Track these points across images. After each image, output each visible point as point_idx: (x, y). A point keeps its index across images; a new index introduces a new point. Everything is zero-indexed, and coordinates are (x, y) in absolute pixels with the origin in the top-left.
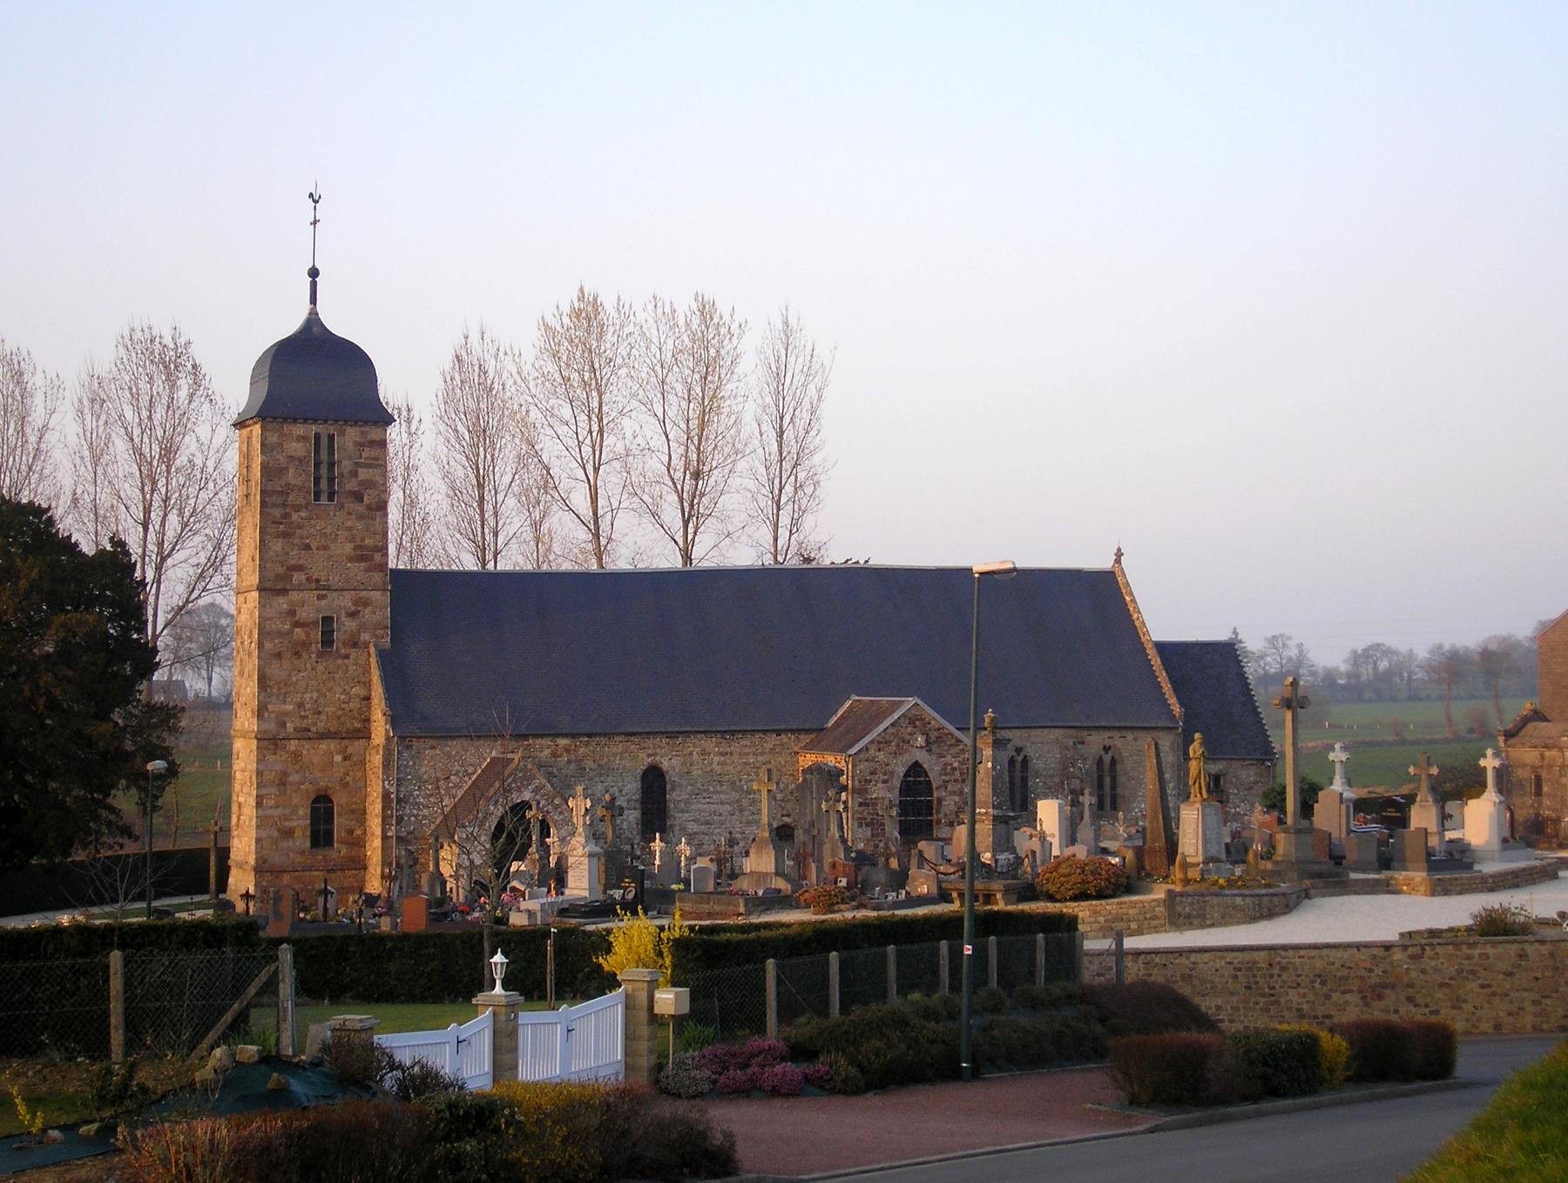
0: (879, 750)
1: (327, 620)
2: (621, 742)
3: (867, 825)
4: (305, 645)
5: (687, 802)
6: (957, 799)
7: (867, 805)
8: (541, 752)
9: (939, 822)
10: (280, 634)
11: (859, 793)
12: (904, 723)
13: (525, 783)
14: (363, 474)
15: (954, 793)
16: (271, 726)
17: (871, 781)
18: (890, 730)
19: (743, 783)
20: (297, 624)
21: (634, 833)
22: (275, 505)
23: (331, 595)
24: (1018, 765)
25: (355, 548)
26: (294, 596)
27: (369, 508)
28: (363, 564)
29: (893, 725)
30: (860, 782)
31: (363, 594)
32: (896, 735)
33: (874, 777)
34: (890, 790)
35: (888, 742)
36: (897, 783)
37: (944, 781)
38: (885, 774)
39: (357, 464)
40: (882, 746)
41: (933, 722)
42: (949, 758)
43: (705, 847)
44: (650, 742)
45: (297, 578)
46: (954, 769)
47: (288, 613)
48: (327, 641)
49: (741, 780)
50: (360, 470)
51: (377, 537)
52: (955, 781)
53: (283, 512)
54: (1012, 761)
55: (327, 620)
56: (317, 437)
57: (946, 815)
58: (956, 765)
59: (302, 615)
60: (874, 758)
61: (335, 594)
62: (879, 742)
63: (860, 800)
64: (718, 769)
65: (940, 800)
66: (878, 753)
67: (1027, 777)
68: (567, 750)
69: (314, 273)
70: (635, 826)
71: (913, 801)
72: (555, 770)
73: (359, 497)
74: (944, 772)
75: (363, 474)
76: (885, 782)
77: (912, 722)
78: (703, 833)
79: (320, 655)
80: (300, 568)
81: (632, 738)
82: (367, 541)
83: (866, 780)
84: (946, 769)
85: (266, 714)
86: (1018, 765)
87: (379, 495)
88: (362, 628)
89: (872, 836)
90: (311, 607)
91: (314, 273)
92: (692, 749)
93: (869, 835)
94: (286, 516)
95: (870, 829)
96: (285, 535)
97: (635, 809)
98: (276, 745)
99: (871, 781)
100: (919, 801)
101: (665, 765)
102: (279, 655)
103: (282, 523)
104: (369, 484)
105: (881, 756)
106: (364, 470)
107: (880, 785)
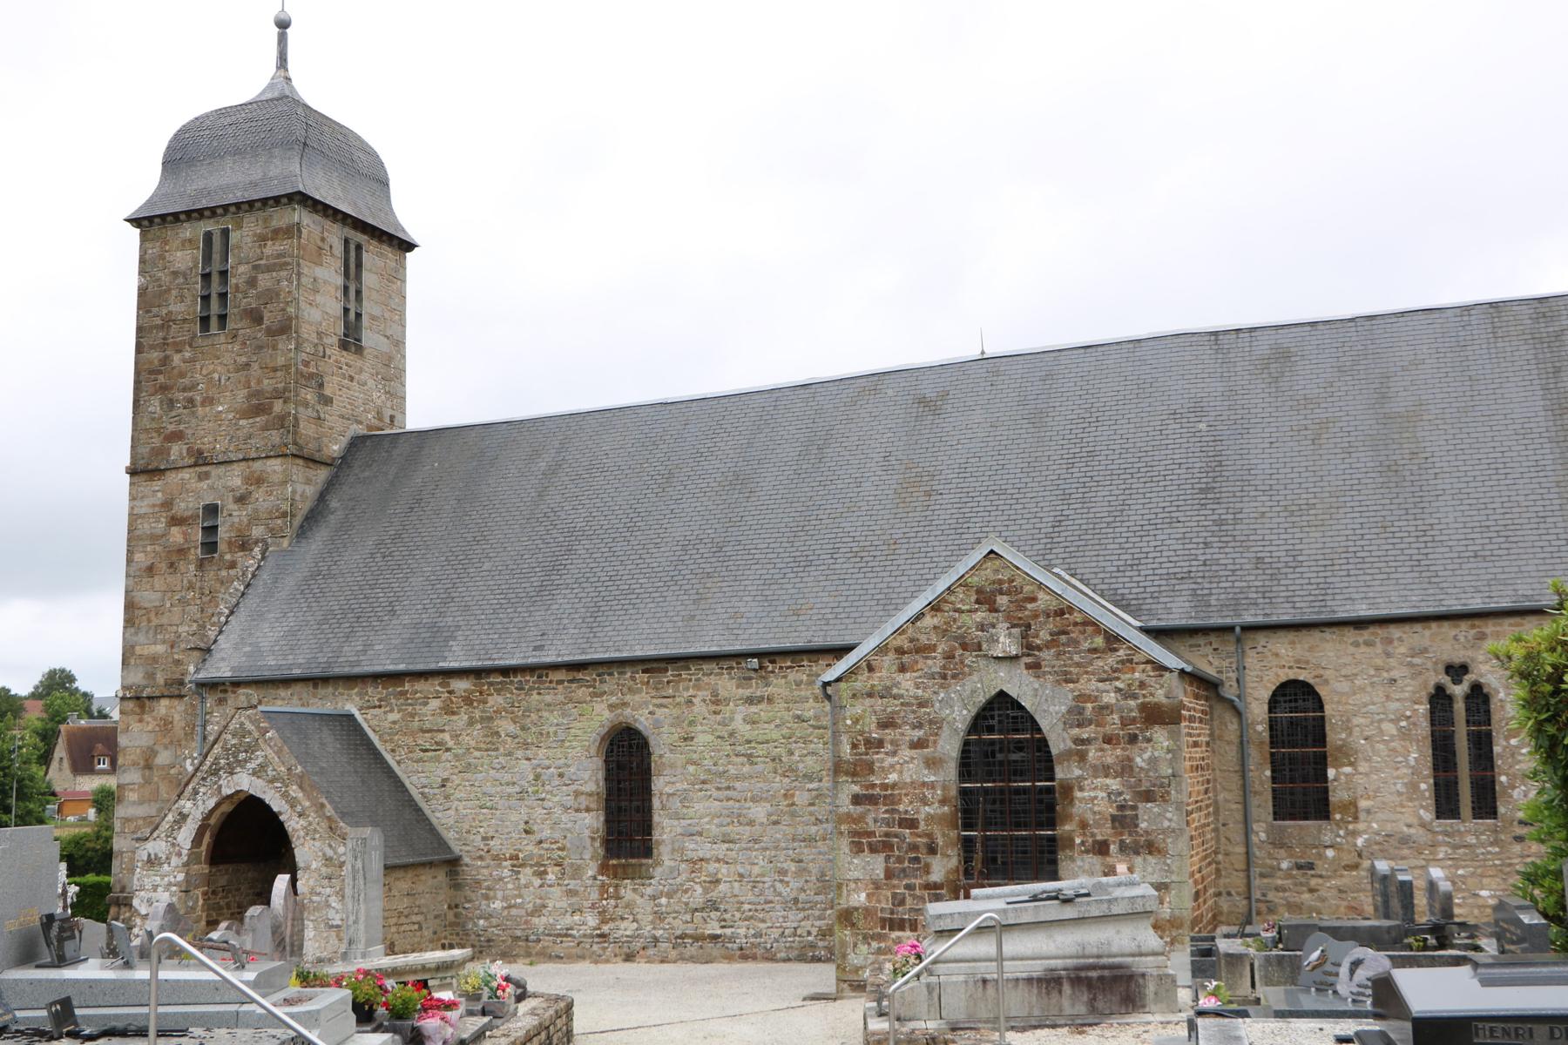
0: (902, 669)
1: (212, 510)
2: (560, 682)
3: (873, 849)
4: (182, 552)
5: (685, 799)
6: (1114, 784)
7: (872, 800)
8: (426, 704)
9: (1070, 843)
10: (154, 538)
11: (854, 774)
12: (964, 600)
13: (242, 756)
14: (264, 281)
15: (1106, 770)
16: (137, 677)
17: (880, 743)
18: (929, 621)
19: (796, 758)
20: (175, 521)
21: (587, 856)
22: (152, 347)
23: (215, 471)
24: (1459, 707)
25: (249, 396)
26: (173, 478)
27: (271, 332)
28: (258, 419)
29: (935, 607)
30: (854, 746)
31: (257, 465)
32: (942, 632)
33: (889, 734)
34: (932, 763)
35: (924, 650)
36: (949, 746)
37: (1079, 741)
38: (920, 726)
39: (256, 267)
40: (906, 659)
41: (1041, 595)
42: (1089, 685)
43: (722, 887)
44: (610, 683)
45: (177, 450)
46: (1104, 709)
47: (162, 505)
48: (210, 547)
49: (791, 753)
50: (260, 277)
51: (279, 374)
52: (1108, 740)
53: (162, 355)
54: (1440, 699)
55: (212, 510)
56: (208, 237)
57: (1084, 825)
58: (1110, 698)
59: (183, 506)
60: (888, 689)
61: (222, 469)
62: (900, 651)
63: (856, 789)
64: (744, 730)
65: (1067, 789)
66: (900, 677)
67: (1489, 735)
68: (468, 701)
69: (283, 25)
70: (588, 841)
71: (1002, 791)
72: (446, 737)
73: (256, 317)
74: (1076, 717)
75: (264, 281)
76: (918, 745)
77: (985, 599)
78: (718, 860)
79: (201, 565)
80: (177, 436)
81: (580, 676)
82: (266, 382)
83: (869, 743)
84: (1081, 711)
85: (132, 662)
86: (1459, 707)
87: (283, 310)
88: (254, 519)
89: (889, 874)
90: (193, 491)
91: (283, 25)
92: (691, 692)
93: (880, 873)
94: (165, 361)
95: (880, 858)
96: (164, 388)
97: (588, 810)
98: (142, 707)
99: (880, 743)
100: (1018, 791)
101: (643, 722)
102: (150, 570)
103: (160, 372)
104: (271, 296)
105: (907, 684)
106: (266, 276)
107: (906, 753)
